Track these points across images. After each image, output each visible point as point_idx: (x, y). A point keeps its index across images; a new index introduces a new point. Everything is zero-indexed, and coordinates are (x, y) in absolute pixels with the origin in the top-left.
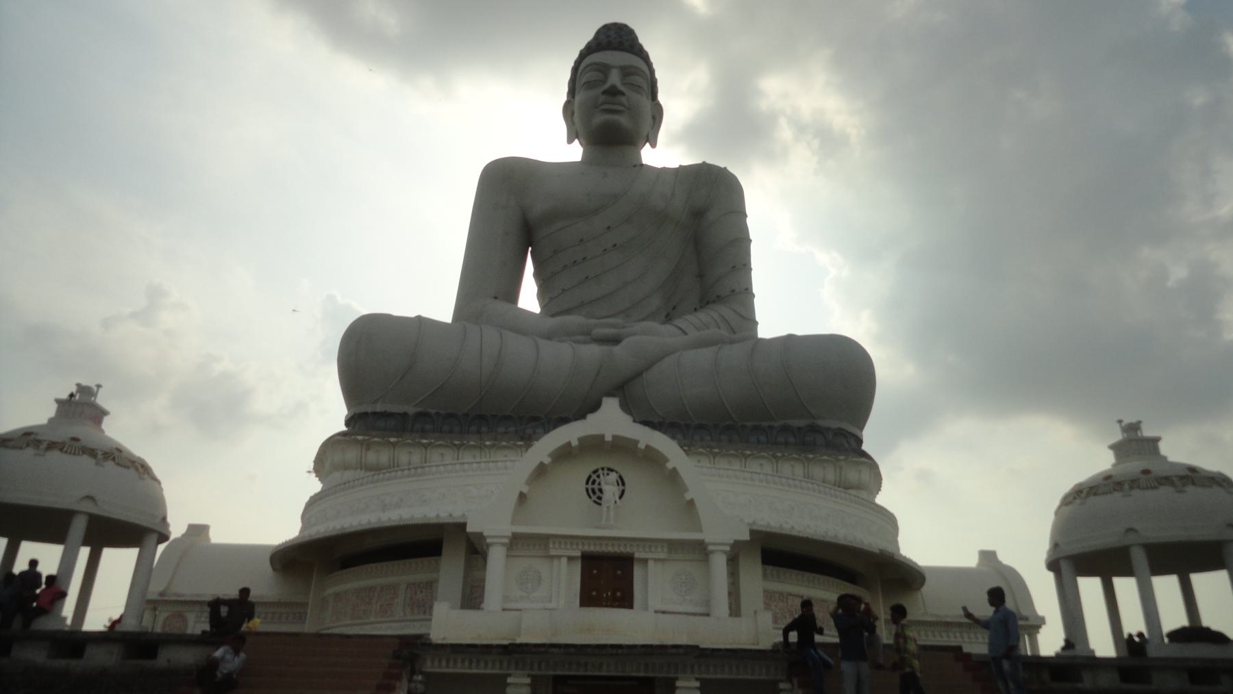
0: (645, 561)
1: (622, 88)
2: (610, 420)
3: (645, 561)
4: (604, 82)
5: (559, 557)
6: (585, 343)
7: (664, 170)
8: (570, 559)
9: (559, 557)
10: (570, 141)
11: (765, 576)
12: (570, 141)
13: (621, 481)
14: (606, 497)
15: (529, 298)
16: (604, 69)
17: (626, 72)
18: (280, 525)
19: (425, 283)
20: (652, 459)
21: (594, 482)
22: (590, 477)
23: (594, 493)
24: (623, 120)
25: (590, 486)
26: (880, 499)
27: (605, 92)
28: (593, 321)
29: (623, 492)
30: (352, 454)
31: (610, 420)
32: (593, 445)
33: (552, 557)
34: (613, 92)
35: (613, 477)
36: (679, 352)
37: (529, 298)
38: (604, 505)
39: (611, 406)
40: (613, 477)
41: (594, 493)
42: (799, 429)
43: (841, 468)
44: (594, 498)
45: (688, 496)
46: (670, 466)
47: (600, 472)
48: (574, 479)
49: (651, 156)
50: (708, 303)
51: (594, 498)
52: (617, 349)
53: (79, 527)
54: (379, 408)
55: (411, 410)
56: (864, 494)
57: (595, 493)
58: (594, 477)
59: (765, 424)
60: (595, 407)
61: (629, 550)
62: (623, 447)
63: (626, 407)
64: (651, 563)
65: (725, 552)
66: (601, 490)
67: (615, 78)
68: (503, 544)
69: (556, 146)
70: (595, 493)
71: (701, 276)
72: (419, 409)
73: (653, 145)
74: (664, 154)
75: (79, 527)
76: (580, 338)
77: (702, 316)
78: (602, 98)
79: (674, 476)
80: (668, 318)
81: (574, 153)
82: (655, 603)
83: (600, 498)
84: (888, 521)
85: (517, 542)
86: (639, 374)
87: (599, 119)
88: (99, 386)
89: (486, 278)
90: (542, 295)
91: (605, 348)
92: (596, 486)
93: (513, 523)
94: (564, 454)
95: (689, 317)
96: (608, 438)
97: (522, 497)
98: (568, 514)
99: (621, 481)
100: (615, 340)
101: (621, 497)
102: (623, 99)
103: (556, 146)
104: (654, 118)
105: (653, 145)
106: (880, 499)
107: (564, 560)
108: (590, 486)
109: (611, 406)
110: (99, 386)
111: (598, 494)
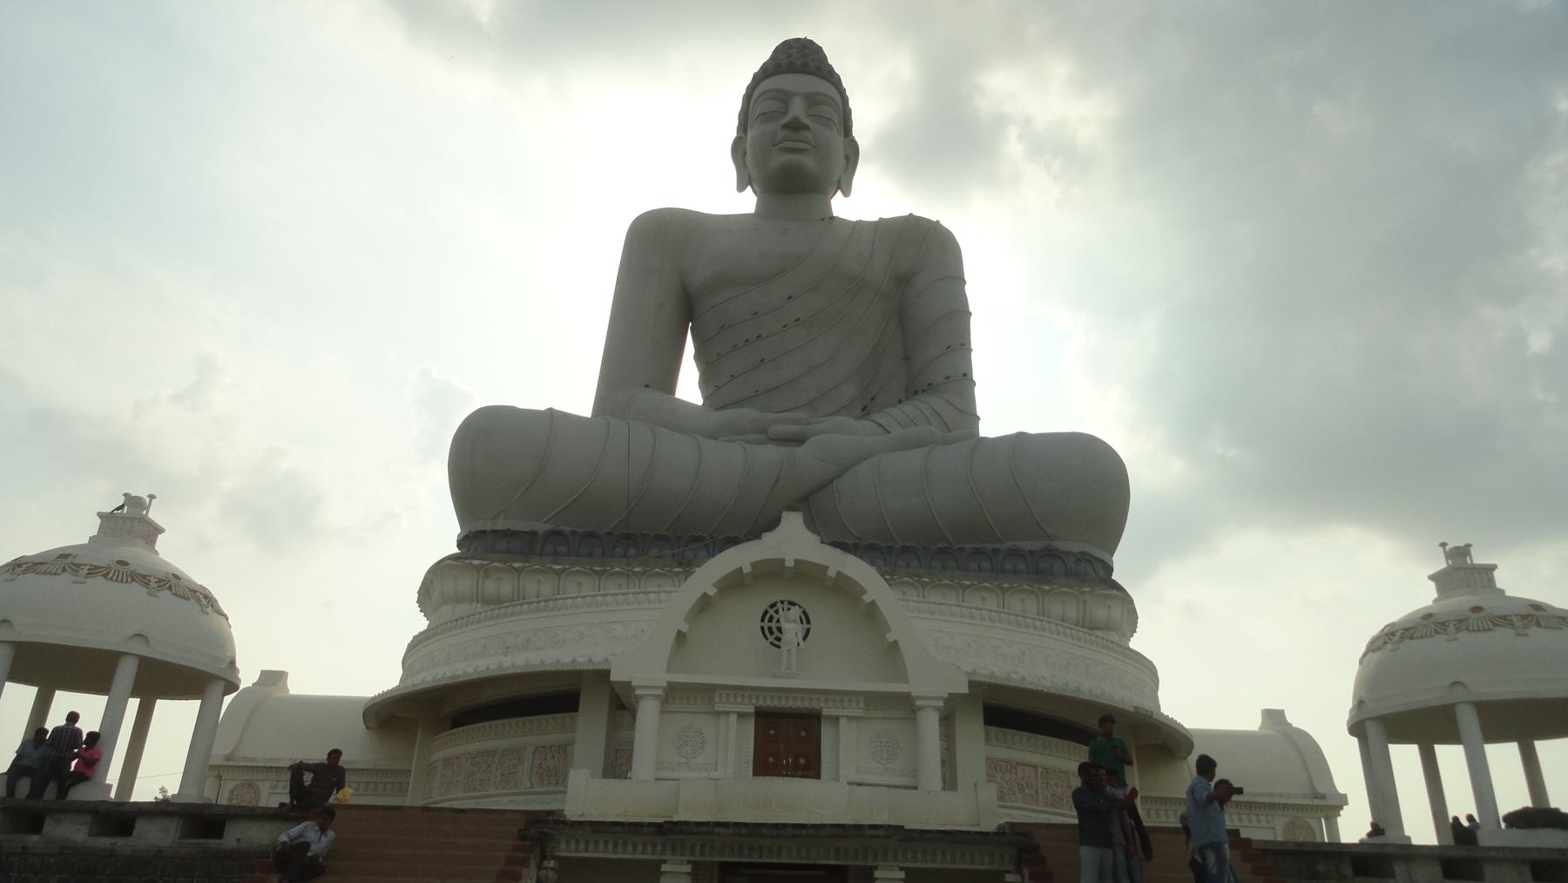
0: (836, 719)
1: (806, 121)
2: (793, 540)
3: (836, 719)
4: (785, 114)
5: (727, 713)
6: (759, 443)
7: (859, 225)
8: (741, 715)
9: (727, 713)
10: (741, 188)
11: (988, 739)
12: (741, 188)
13: (806, 618)
14: (786, 637)
15: (689, 386)
16: (784, 97)
17: (812, 101)
18: (380, 675)
19: (557, 366)
20: (844, 589)
21: (771, 620)
22: (766, 612)
23: (771, 632)
24: (808, 161)
25: (766, 624)
26: (1135, 643)
27: (785, 127)
28: (771, 416)
29: (808, 631)
30: (466, 584)
31: (793, 540)
32: (770, 572)
33: (719, 713)
34: (795, 126)
35: (795, 612)
36: (881, 459)
37: (689, 386)
38: (784, 648)
39: (793, 523)
40: (795, 612)
41: (771, 632)
42: (1032, 552)
43: (1085, 602)
44: (771, 639)
45: (890, 637)
46: (867, 598)
47: (779, 606)
48: (746, 614)
49: (843, 207)
50: (916, 392)
51: (771, 639)
52: (800, 450)
53: (126, 673)
54: (500, 525)
55: (541, 527)
56: (1114, 637)
57: (772, 634)
58: (771, 612)
59: (989, 546)
60: (773, 524)
61: (815, 705)
62: (806, 574)
63: (811, 524)
64: (843, 722)
65: (937, 708)
66: (779, 630)
67: (797, 109)
68: (657, 697)
69: (724, 195)
70: (772, 634)
71: (907, 358)
72: (549, 527)
73: (846, 194)
74: (868, 199)
75: (126, 673)
76: (752, 437)
77: (909, 409)
78: (781, 134)
79: (871, 614)
80: (865, 412)
81: (746, 203)
82: (849, 772)
83: (778, 639)
84: (1146, 671)
85: (674, 694)
86: (830, 482)
87: (778, 160)
88: (152, 497)
89: (634, 361)
90: (705, 382)
91: (785, 450)
92: (773, 625)
93: (669, 670)
94: (733, 584)
95: (893, 411)
96: (790, 563)
97: (680, 636)
98: (739, 661)
99: (806, 618)
100: (798, 440)
101: (804, 639)
102: (808, 135)
103: (724, 195)
104: (847, 158)
105: (846, 194)
106: (1135, 643)
107: (733, 717)
108: (766, 624)
109: (793, 523)
110: (152, 497)
111: (776, 633)
